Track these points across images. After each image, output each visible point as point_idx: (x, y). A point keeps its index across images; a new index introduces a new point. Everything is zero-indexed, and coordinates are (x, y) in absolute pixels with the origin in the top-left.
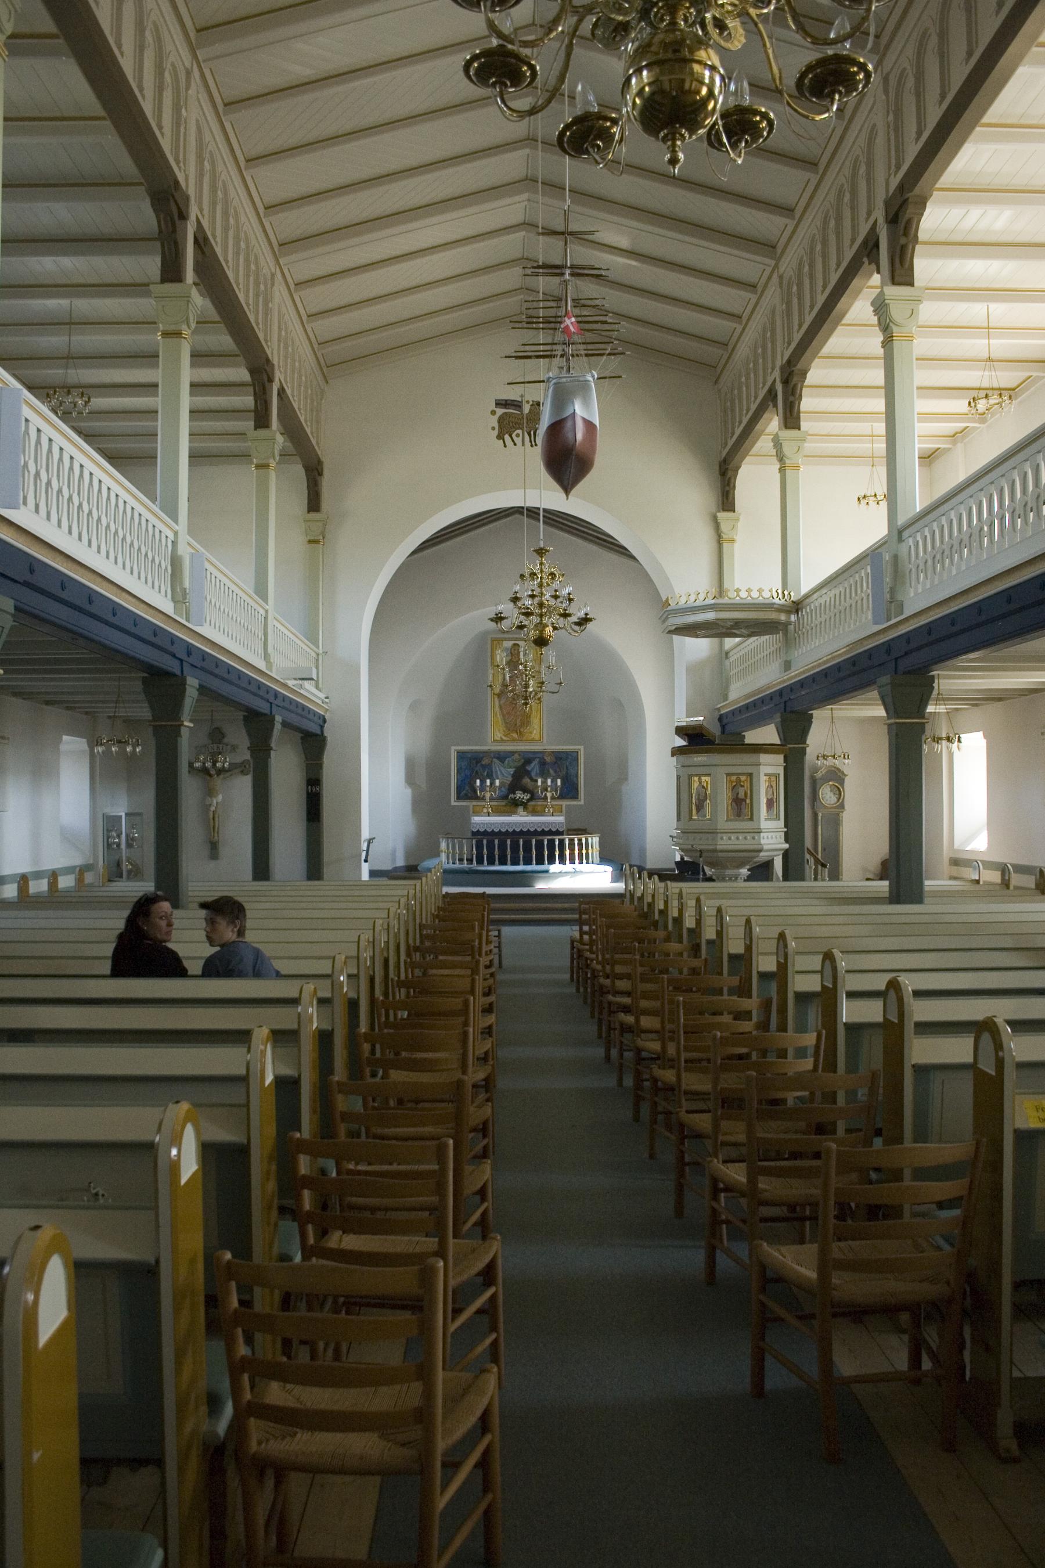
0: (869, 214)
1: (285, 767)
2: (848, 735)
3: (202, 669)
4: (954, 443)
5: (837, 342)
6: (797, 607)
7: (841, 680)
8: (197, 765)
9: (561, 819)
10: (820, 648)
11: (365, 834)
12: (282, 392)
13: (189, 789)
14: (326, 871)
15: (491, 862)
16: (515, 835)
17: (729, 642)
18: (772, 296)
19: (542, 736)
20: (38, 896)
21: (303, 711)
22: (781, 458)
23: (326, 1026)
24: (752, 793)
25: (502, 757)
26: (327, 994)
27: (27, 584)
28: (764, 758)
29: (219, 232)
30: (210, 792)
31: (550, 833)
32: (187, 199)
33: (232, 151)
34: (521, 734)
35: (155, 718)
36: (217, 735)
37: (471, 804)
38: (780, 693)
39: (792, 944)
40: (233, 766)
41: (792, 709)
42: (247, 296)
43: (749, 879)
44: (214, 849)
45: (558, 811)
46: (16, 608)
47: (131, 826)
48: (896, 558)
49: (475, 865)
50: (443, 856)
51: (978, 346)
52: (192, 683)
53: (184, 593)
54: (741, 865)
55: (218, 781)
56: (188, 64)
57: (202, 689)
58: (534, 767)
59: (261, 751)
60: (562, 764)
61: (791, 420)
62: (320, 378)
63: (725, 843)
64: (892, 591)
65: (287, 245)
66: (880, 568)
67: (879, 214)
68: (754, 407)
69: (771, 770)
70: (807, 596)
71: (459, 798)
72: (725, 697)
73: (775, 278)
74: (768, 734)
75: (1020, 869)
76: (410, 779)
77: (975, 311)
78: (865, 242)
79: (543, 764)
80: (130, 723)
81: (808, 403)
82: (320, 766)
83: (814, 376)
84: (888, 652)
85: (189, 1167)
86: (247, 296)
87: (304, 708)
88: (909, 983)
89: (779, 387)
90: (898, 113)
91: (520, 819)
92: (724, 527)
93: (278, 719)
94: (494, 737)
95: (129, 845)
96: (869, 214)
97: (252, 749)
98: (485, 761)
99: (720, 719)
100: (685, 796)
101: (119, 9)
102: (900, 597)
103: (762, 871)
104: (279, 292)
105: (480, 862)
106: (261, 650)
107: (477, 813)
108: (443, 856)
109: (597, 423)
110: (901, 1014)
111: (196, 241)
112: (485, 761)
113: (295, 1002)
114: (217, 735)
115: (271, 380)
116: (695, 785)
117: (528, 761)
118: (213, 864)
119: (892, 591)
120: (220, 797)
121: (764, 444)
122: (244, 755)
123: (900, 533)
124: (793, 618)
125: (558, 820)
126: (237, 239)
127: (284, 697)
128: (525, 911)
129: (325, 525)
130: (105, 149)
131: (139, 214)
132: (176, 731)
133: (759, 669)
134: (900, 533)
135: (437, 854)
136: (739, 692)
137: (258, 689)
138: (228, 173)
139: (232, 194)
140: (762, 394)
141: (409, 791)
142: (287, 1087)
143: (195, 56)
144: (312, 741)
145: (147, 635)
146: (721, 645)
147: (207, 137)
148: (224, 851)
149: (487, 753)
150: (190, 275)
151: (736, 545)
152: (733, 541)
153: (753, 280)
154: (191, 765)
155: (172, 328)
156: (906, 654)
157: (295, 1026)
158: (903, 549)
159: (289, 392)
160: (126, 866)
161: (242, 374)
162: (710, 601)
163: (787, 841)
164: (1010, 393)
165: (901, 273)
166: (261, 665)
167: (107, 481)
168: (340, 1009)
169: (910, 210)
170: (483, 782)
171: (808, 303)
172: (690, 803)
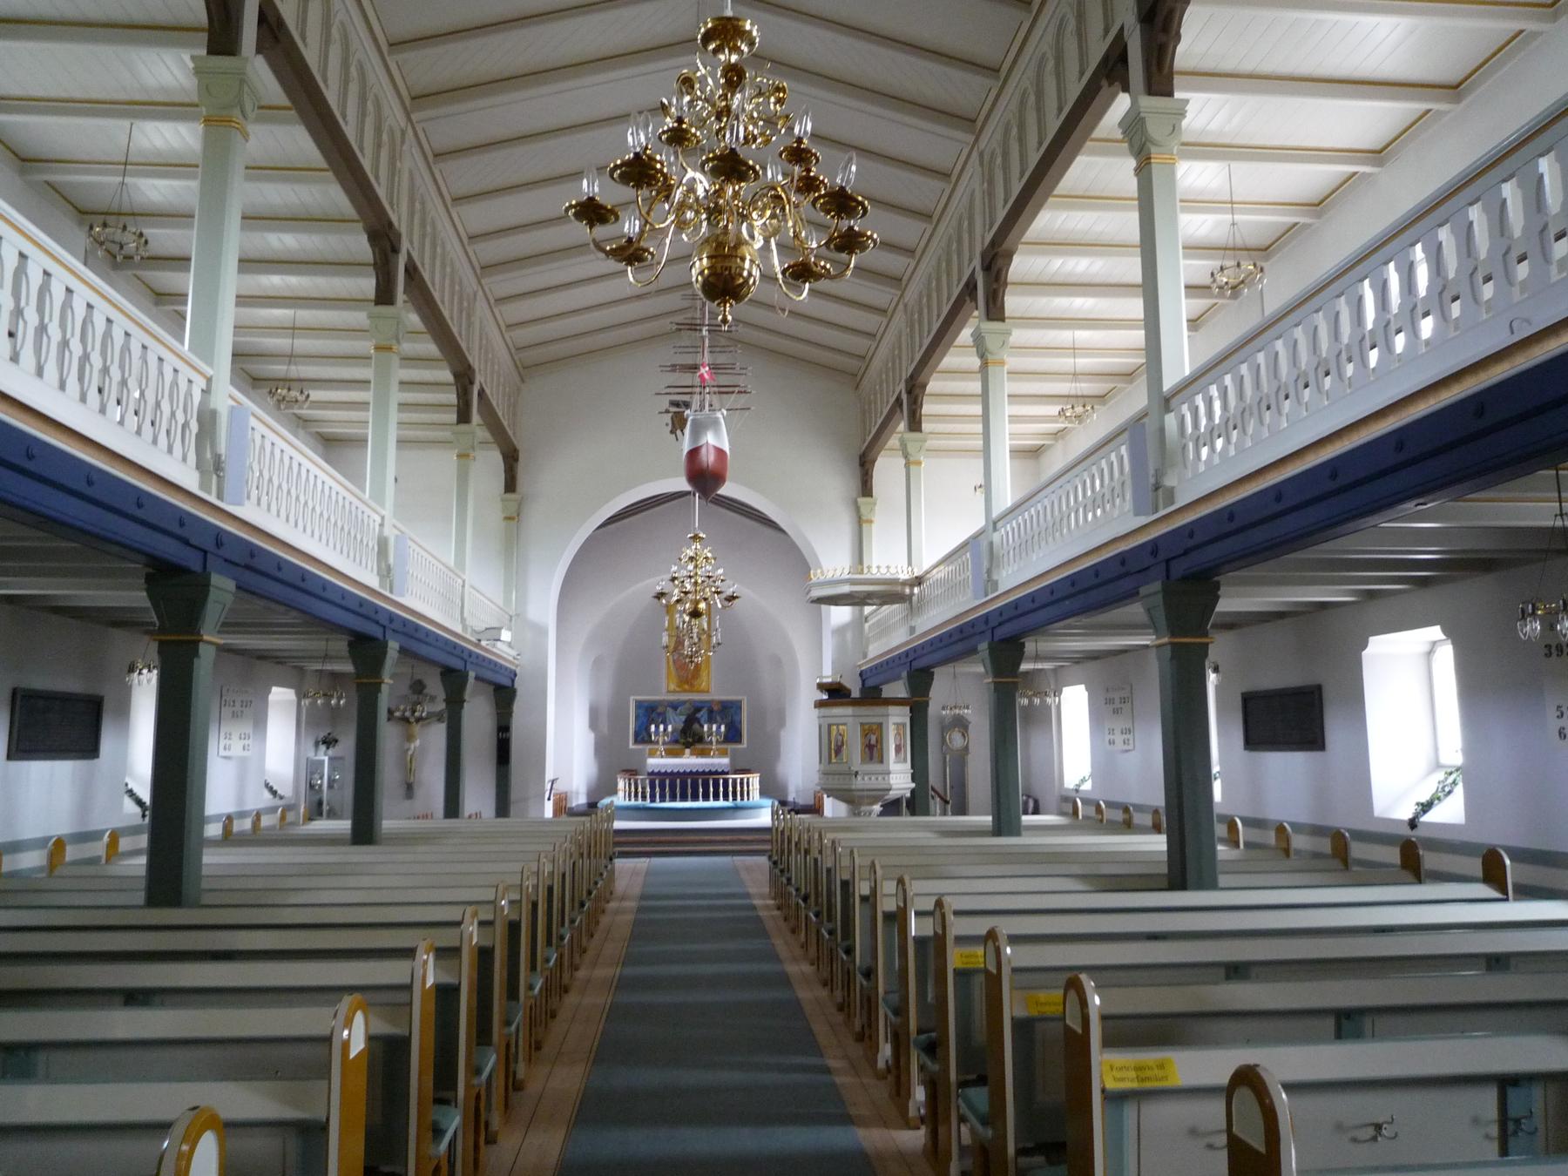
0: (971, 260)
1: (477, 715)
2: (961, 692)
3: (405, 634)
4: (1056, 440)
5: (950, 360)
6: (919, 581)
7: (955, 642)
8: (397, 714)
9: (725, 761)
10: (936, 617)
11: (549, 776)
12: (482, 393)
13: (388, 735)
14: (513, 809)
15: (663, 799)
16: (683, 775)
17: (868, 609)
18: (899, 320)
19: (714, 689)
20: (242, 833)
21: (496, 667)
22: (906, 456)
23: (487, 943)
24: (880, 740)
25: (675, 706)
26: (490, 917)
27: (248, 567)
28: (892, 709)
29: (427, 260)
30: (409, 738)
31: (716, 773)
32: (399, 236)
33: (439, 189)
34: (692, 685)
35: (358, 675)
36: (418, 687)
37: (648, 747)
38: (907, 653)
39: (879, 872)
40: (430, 715)
41: (917, 670)
42: (452, 311)
43: (882, 814)
44: (409, 790)
45: (723, 753)
46: (238, 587)
47: (332, 769)
48: (991, 544)
49: (648, 803)
50: (621, 794)
51: (1066, 363)
52: (393, 645)
53: (389, 569)
54: (874, 800)
55: (416, 728)
56: (403, 124)
57: (403, 651)
58: (703, 715)
59: (455, 702)
60: (727, 713)
61: (915, 424)
62: (517, 379)
63: (860, 783)
64: (989, 572)
65: (488, 268)
66: (978, 552)
67: (977, 262)
68: (885, 412)
69: (898, 720)
70: (927, 572)
71: (636, 741)
72: (865, 656)
73: (901, 306)
74: (898, 689)
75: (1110, 804)
76: (593, 724)
77: (1065, 336)
78: (967, 285)
79: (711, 711)
80: (335, 676)
81: (928, 408)
82: (510, 714)
83: (933, 386)
84: (987, 622)
85: (358, 1046)
86: (433, 273)
87: (496, 664)
88: (952, 904)
89: (904, 397)
90: (991, 182)
91: (688, 761)
92: (863, 510)
93: (472, 675)
94: (664, 689)
95: (330, 786)
96: (971, 260)
97: (448, 701)
98: (660, 710)
99: (861, 674)
100: (825, 741)
101: (363, 122)
102: (995, 577)
103: (892, 808)
104: (481, 308)
105: (653, 800)
106: (458, 615)
107: (652, 754)
108: (621, 794)
109: (726, 448)
110: (944, 927)
111: (406, 270)
112: (660, 710)
113: (458, 924)
114: (418, 687)
115: (472, 383)
116: (834, 733)
117: (698, 710)
118: (407, 803)
119: (989, 572)
120: (418, 743)
121: (894, 441)
122: (440, 706)
123: (995, 524)
124: (916, 590)
125: (723, 762)
126: (434, 246)
127: (478, 656)
128: (649, 843)
129: (520, 505)
130: (331, 195)
131: (358, 245)
132: (376, 688)
133: (892, 634)
134: (995, 524)
135: (614, 792)
136: (877, 649)
137: (453, 648)
138: (436, 209)
139: (439, 227)
140: (892, 400)
141: (592, 736)
142: (446, 995)
143: (409, 119)
144: (504, 694)
145: (353, 605)
146: (861, 612)
147: (418, 182)
148: (419, 792)
149: (660, 703)
150: (401, 296)
151: (874, 526)
152: (871, 522)
153: (885, 306)
154: (390, 712)
155: (384, 343)
156: (1186, 553)
157: (457, 944)
158: (996, 537)
159: (488, 391)
160: (325, 808)
161: (446, 375)
162: (845, 576)
163: (913, 780)
164: (1101, 398)
165: (995, 311)
166: (458, 629)
167: (322, 476)
168: (500, 930)
169: (1000, 262)
170: (657, 727)
171: (955, 278)
172: (832, 748)
